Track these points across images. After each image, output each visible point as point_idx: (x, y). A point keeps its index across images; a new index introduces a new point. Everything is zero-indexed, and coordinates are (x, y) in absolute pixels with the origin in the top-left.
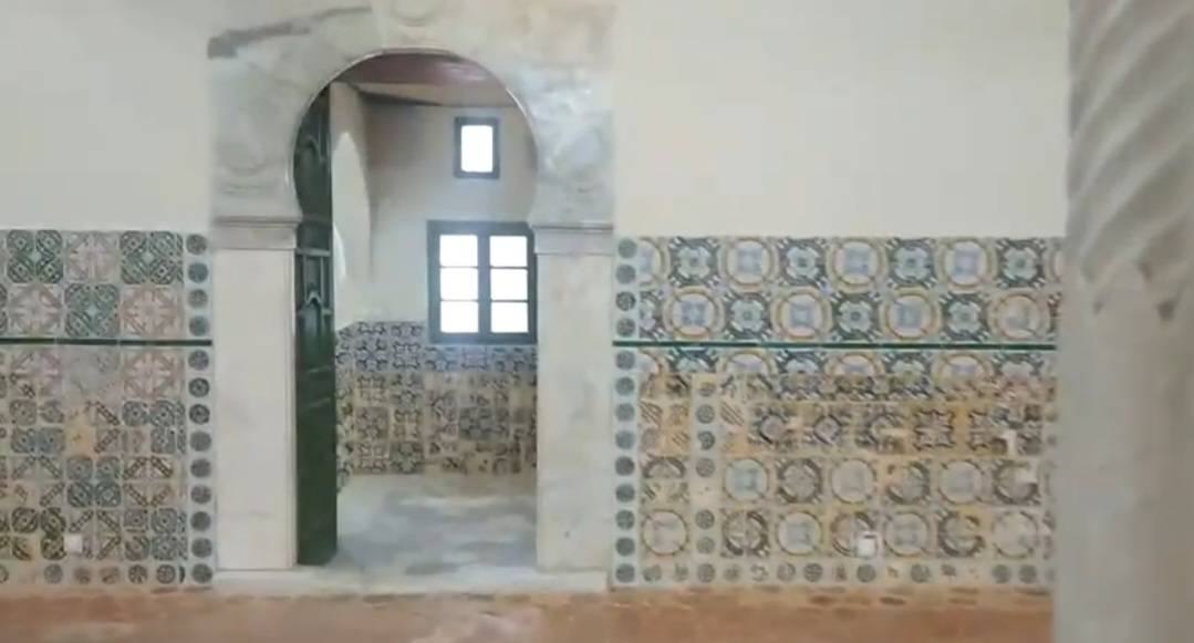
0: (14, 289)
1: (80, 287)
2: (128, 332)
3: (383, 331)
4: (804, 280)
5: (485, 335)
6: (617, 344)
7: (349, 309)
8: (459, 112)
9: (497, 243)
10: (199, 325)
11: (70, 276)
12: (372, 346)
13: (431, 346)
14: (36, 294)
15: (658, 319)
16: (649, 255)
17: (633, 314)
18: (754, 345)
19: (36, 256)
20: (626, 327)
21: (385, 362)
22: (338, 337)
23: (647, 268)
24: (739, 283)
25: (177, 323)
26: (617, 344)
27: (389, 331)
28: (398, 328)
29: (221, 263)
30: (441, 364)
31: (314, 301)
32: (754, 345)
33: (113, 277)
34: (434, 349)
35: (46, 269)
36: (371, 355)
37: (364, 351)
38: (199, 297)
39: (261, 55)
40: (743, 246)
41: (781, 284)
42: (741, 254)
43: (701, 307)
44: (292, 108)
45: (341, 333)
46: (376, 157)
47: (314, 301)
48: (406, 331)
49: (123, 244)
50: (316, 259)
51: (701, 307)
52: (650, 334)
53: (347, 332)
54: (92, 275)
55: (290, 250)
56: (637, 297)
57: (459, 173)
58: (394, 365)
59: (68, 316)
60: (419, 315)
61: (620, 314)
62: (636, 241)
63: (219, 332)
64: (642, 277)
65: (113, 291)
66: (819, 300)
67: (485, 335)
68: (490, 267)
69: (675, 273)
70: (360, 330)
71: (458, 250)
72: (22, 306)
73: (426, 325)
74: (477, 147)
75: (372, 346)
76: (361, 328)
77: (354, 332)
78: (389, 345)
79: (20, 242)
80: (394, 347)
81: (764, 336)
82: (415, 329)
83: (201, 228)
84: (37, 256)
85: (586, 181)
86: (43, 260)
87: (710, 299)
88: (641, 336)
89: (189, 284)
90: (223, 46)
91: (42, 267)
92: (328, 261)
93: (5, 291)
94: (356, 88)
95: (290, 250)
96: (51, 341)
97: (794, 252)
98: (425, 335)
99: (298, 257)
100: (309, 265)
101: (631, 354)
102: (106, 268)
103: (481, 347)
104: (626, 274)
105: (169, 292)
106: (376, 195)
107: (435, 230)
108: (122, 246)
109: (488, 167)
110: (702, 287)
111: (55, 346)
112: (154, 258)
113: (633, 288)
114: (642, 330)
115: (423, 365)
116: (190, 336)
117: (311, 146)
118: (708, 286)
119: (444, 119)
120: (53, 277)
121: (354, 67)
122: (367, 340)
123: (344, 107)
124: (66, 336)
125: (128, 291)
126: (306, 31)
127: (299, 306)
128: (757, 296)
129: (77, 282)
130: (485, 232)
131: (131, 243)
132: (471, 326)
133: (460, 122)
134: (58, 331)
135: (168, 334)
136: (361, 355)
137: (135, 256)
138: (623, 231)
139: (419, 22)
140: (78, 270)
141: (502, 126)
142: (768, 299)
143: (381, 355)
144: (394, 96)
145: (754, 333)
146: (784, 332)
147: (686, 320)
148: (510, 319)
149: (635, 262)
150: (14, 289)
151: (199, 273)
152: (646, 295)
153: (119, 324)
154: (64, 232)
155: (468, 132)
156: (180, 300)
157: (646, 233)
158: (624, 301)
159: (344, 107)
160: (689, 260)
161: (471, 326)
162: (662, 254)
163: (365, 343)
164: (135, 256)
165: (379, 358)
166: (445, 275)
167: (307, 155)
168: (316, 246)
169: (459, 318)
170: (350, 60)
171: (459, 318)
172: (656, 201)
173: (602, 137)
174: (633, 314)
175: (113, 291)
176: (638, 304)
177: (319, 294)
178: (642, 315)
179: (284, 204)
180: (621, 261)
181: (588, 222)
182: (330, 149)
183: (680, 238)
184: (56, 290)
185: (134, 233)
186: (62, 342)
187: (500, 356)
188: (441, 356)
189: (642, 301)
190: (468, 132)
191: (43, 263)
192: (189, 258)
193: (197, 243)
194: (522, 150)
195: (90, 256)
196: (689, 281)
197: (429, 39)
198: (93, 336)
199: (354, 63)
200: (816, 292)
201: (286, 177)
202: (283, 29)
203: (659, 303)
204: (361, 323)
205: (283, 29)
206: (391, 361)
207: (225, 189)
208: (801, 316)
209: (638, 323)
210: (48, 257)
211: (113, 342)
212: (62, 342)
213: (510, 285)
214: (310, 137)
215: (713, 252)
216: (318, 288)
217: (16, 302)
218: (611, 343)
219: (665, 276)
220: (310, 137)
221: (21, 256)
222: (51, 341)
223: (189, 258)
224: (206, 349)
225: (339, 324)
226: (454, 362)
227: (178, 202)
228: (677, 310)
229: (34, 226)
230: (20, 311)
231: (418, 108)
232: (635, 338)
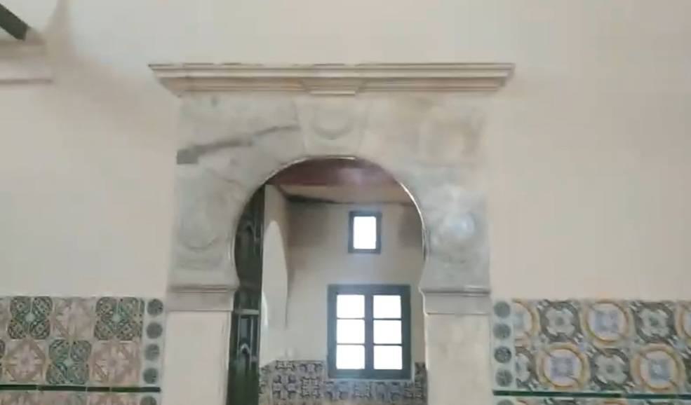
0: (11, 344)
1: (62, 342)
2: (95, 381)
3: (294, 368)
4: (656, 339)
5: (370, 371)
6: (498, 393)
7: (268, 355)
8: (353, 208)
9: (378, 299)
10: (151, 375)
11: (55, 334)
12: (285, 380)
13: (328, 380)
14: (27, 348)
15: (531, 370)
16: (520, 315)
17: (510, 367)
18: (617, 396)
19: (30, 318)
20: (504, 378)
21: (294, 392)
22: (261, 373)
23: (520, 327)
24: (600, 340)
25: (134, 373)
26: (498, 393)
27: (298, 368)
28: (304, 365)
29: (173, 323)
30: (336, 395)
31: (245, 351)
32: (617, 396)
33: (88, 335)
34: (332, 383)
35: (37, 328)
36: (285, 388)
37: (279, 384)
38: (153, 352)
39: (218, 162)
40: (603, 308)
41: (637, 341)
42: (600, 314)
43: (569, 361)
44: (237, 199)
45: (263, 369)
46: (294, 239)
47: (245, 351)
48: (311, 368)
49: (99, 305)
50: (248, 317)
51: (569, 361)
52: (525, 384)
53: (267, 369)
54: (71, 332)
55: (228, 311)
56: (513, 351)
57: (351, 249)
58: (302, 395)
59: (50, 366)
60: (321, 355)
61: (498, 366)
62: (509, 302)
63: (163, 382)
64: (515, 334)
65: (87, 346)
66: (672, 355)
67: (370, 371)
68: (373, 319)
69: (544, 331)
70: (276, 368)
71: (350, 306)
72: (15, 358)
73: (326, 364)
74: (365, 232)
75: (285, 380)
76: (278, 365)
77: (272, 369)
78: (297, 379)
79: (20, 306)
80: (302, 381)
81: (627, 388)
82: (317, 366)
83: (160, 294)
84: (30, 317)
85: (465, 253)
86: (35, 320)
87: (577, 354)
88: (519, 386)
89: (147, 340)
90: (187, 156)
91: (35, 326)
92: (257, 319)
93: (4, 345)
94: (280, 190)
95: (228, 311)
96: (33, 387)
97: (645, 314)
98: (324, 373)
99: (235, 318)
100: (242, 323)
101: (509, 402)
102: (80, 326)
103: (367, 381)
104: (502, 332)
105: (130, 346)
106: (293, 267)
107: (334, 292)
108: (97, 310)
109: (373, 246)
110: (569, 344)
111: (37, 392)
112: (121, 319)
113: (509, 344)
114: (518, 380)
115: (322, 395)
116: (142, 383)
117: (249, 229)
118: (574, 342)
119: (343, 212)
120: (42, 334)
121: (285, 169)
122: (280, 374)
123: (273, 201)
124: (47, 384)
125: (97, 346)
126: (250, 144)
127: (233, 354)
128: (616, 352)
129: (59, 338)
130: (369, 293)
131: (106, 307)
132: (360, 364)
133: (352, 215)
134: (40, 379)
135: (126, 383)
136: (278, 387)
137: (106, 318)
138: (501, 293)
139: (332, 135)
140: (61, 329)
141: (384, 219)
142: (544, 336)
143: (291, 387)
144: (304, 194)
145: (616, 384)
146: (645, 384)
147: (556, 372)
148: (388, 359)
149: (510, 321)
150: (11, 344)
151: (155, 331)
152: (520, 350)
153: (88, 371)
154: (55, 298)
155: (358, 221)
156: (138, 352)
157: (519, 296)
158: (502, 355)
159: (273, 201)
160: (558, 319)
161: (360, 364)
162: (588, 329)
163: (289, 397)
164: (106, 318)
165: (289, 389)
166: (340, 325)
167: (245, 237)
168: (250, 307)
169: (350, 358)
170: (283, 164)
171: (350, 358)
172: (528, 267)
173: (478, 216)
174: (510, 367)
175: (87, 346)
176: (514, 358)
177: (249, 346)
178: (518, 367)
179: (226, 275)
180: (497, 320)
181: (469, 287)
182: (263, 233)
183: (546, 301)
184: (43, 345)
185: (108, 298)
186: (44, 388)
187: (381, 388)
188: (336, 388)
189: (517, 355)
190: (358, 221)
191: (35, 323)
192: (148, 319)
193: (156, 307)
194: (408, 227)
195: (71, 318)
196: (557, 338)
197: (345, 147)
198: (67, 383)
199: (286, 166)
200: (668, 348)
201: (229, 256)
202: (233, 143)
203: (531, 357)
204: (277, 362)
205: (233, 143)
206: (299, 391)
207: (181, 262)
208: (658, 369)
209: (514, 375)
210: (41, 319)
211: (83, 389)
212: (44, 388)
213: (388, 332)
214: (249, 223)
215: (576, 312)
216: (247, 341)
217: (11, 354)
218: (491, 393)
219: (536, 334)
220: (249, 223)
221: (19, 317)
222: (33, 387)
223: (148, 319)
224: (154, 395)
225: (263, 363)
226: (346, 393)
227: (143, 278)
228: (549, 364)
229: (31, 292)
230: (13, 362)
231: (328, 205)
232: (513, 387)
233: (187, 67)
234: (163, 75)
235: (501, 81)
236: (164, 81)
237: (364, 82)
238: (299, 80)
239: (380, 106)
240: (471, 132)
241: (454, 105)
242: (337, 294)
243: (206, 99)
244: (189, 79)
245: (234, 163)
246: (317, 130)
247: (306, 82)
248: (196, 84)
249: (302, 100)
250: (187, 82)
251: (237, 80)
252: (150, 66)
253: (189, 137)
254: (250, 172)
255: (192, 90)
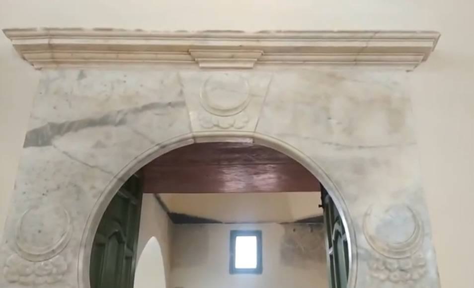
57: (233, 270)
90: (38, 138)
126: (122, 122)
133: (233, 235)
139: (225, 112)
141: (254, 276)
170: (164, 147)
190: (240, 241)
233: (50, 33)
234: (19, 42)
235: (423, 54)
236: (23, 50)
237: (262, 52)
238: (187, 50)
239: (285, 81)
240: (395, 112)
241: (376, 78)
242: (255, 269)
243: (72, 73)
244: (51, 47)
245: (99, 145)
246: (207, 106)
247: (191, 52)
248: (59, 55)
249: (189, 74)
250: (47, 50)
251: (113, 50)
252: (5, 31)
253: (46, 113)
254: (118, 159)
255: (56, 62)
